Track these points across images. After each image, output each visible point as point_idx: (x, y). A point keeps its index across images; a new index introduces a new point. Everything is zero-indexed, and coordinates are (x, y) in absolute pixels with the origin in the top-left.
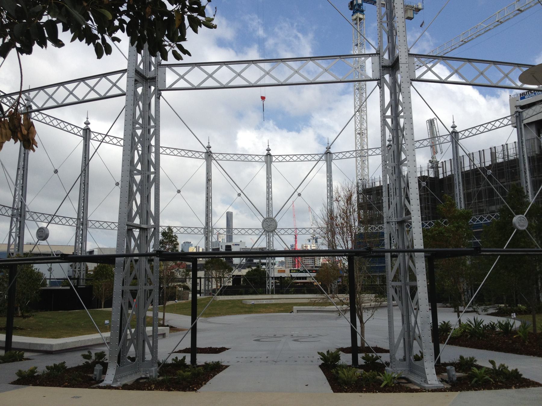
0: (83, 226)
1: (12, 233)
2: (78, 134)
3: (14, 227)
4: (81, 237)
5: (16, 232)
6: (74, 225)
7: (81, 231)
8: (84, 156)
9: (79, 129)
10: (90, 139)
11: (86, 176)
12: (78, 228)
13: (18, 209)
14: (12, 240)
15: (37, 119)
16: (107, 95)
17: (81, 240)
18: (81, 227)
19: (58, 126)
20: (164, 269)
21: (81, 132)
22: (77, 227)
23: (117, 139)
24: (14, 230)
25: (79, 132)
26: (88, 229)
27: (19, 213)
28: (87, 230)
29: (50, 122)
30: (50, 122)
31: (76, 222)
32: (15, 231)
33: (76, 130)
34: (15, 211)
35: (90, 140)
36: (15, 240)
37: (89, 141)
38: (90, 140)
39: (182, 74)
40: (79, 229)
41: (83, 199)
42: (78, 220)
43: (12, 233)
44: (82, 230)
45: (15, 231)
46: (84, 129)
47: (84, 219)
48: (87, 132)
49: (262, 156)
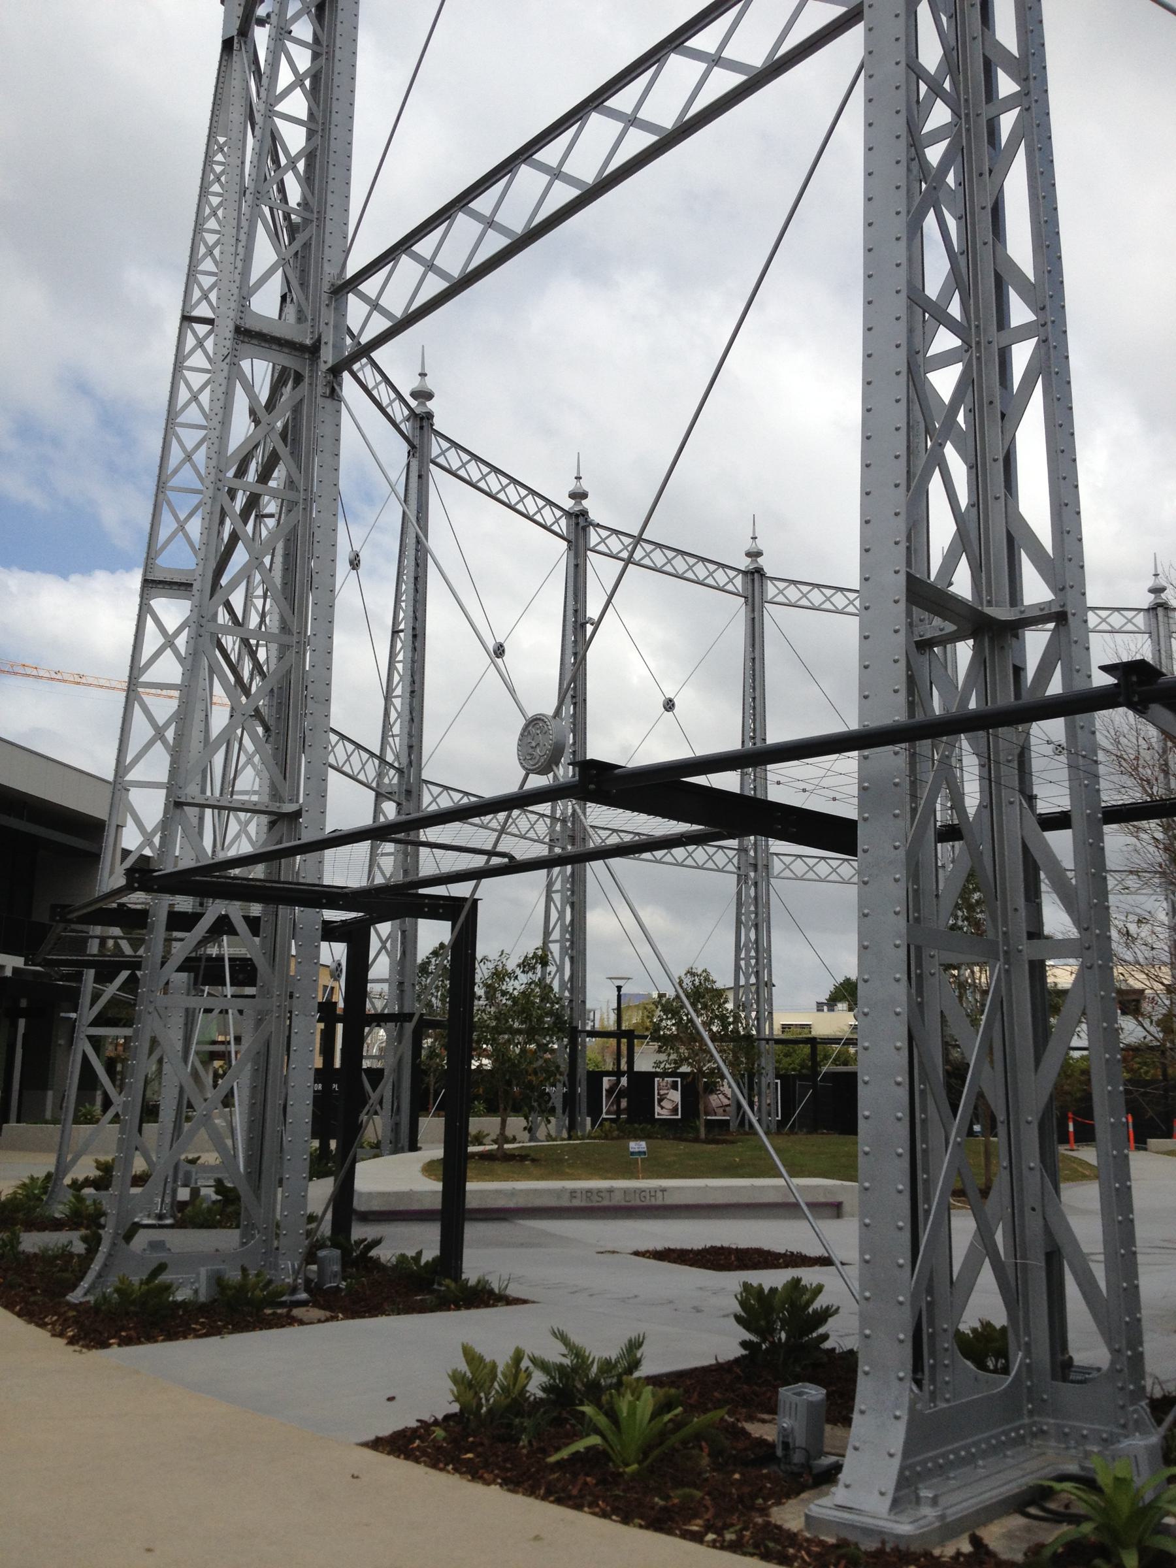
0: (756, 871)
1: (550, 945)
2: (730, 587)
3: (556, 924)
4: (752, 908)
5: (561, 941)
6: (730, 867)
7: (753, 888)
8: (748, 657)
9: (732, 573)
10: (763, 601)
11: (758, 717)
12: (742, 879)
13: (564, 821)
14: (554, 915)
15: (607, 551)
16: (149, 616)
17: (753, 916)
18: (752, 874)
19: (710, 581)
20: (988, 985)
21: (739, 581)
22: (738, 875)
23: (800, 586)
24: (556, 935)
25: (731, 580)
26: (772, 881)
27: (570, 833)
28: (768, 883)
29: (666, 564)
30: (666, 564)
31: (735, 861)
32: (559, 888)
33: (721, 577)
34: (558, 827)
35: (766, 605)
36: (562, 914)
37: (763, 607)
38: (766, 605)
39: (161, 640)
40: (746, 883)
41: (752, 786)
42: (743, 854)
43: (550, 945)
44: (756, 884)
45: (559, 888)
46: (745, 573)
47: (759, 851)
48: (753, 580)
49: (1134, 613)
